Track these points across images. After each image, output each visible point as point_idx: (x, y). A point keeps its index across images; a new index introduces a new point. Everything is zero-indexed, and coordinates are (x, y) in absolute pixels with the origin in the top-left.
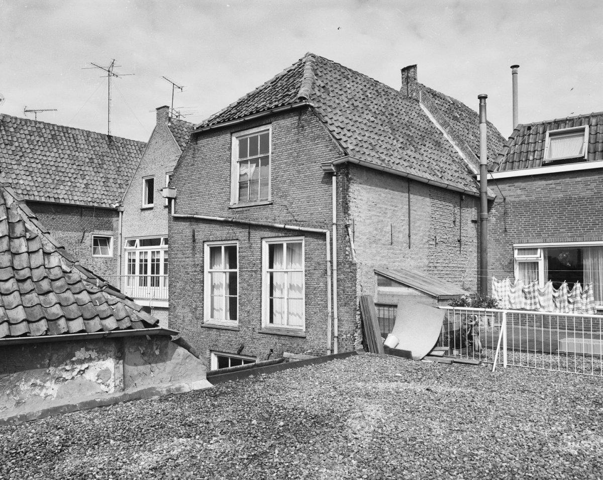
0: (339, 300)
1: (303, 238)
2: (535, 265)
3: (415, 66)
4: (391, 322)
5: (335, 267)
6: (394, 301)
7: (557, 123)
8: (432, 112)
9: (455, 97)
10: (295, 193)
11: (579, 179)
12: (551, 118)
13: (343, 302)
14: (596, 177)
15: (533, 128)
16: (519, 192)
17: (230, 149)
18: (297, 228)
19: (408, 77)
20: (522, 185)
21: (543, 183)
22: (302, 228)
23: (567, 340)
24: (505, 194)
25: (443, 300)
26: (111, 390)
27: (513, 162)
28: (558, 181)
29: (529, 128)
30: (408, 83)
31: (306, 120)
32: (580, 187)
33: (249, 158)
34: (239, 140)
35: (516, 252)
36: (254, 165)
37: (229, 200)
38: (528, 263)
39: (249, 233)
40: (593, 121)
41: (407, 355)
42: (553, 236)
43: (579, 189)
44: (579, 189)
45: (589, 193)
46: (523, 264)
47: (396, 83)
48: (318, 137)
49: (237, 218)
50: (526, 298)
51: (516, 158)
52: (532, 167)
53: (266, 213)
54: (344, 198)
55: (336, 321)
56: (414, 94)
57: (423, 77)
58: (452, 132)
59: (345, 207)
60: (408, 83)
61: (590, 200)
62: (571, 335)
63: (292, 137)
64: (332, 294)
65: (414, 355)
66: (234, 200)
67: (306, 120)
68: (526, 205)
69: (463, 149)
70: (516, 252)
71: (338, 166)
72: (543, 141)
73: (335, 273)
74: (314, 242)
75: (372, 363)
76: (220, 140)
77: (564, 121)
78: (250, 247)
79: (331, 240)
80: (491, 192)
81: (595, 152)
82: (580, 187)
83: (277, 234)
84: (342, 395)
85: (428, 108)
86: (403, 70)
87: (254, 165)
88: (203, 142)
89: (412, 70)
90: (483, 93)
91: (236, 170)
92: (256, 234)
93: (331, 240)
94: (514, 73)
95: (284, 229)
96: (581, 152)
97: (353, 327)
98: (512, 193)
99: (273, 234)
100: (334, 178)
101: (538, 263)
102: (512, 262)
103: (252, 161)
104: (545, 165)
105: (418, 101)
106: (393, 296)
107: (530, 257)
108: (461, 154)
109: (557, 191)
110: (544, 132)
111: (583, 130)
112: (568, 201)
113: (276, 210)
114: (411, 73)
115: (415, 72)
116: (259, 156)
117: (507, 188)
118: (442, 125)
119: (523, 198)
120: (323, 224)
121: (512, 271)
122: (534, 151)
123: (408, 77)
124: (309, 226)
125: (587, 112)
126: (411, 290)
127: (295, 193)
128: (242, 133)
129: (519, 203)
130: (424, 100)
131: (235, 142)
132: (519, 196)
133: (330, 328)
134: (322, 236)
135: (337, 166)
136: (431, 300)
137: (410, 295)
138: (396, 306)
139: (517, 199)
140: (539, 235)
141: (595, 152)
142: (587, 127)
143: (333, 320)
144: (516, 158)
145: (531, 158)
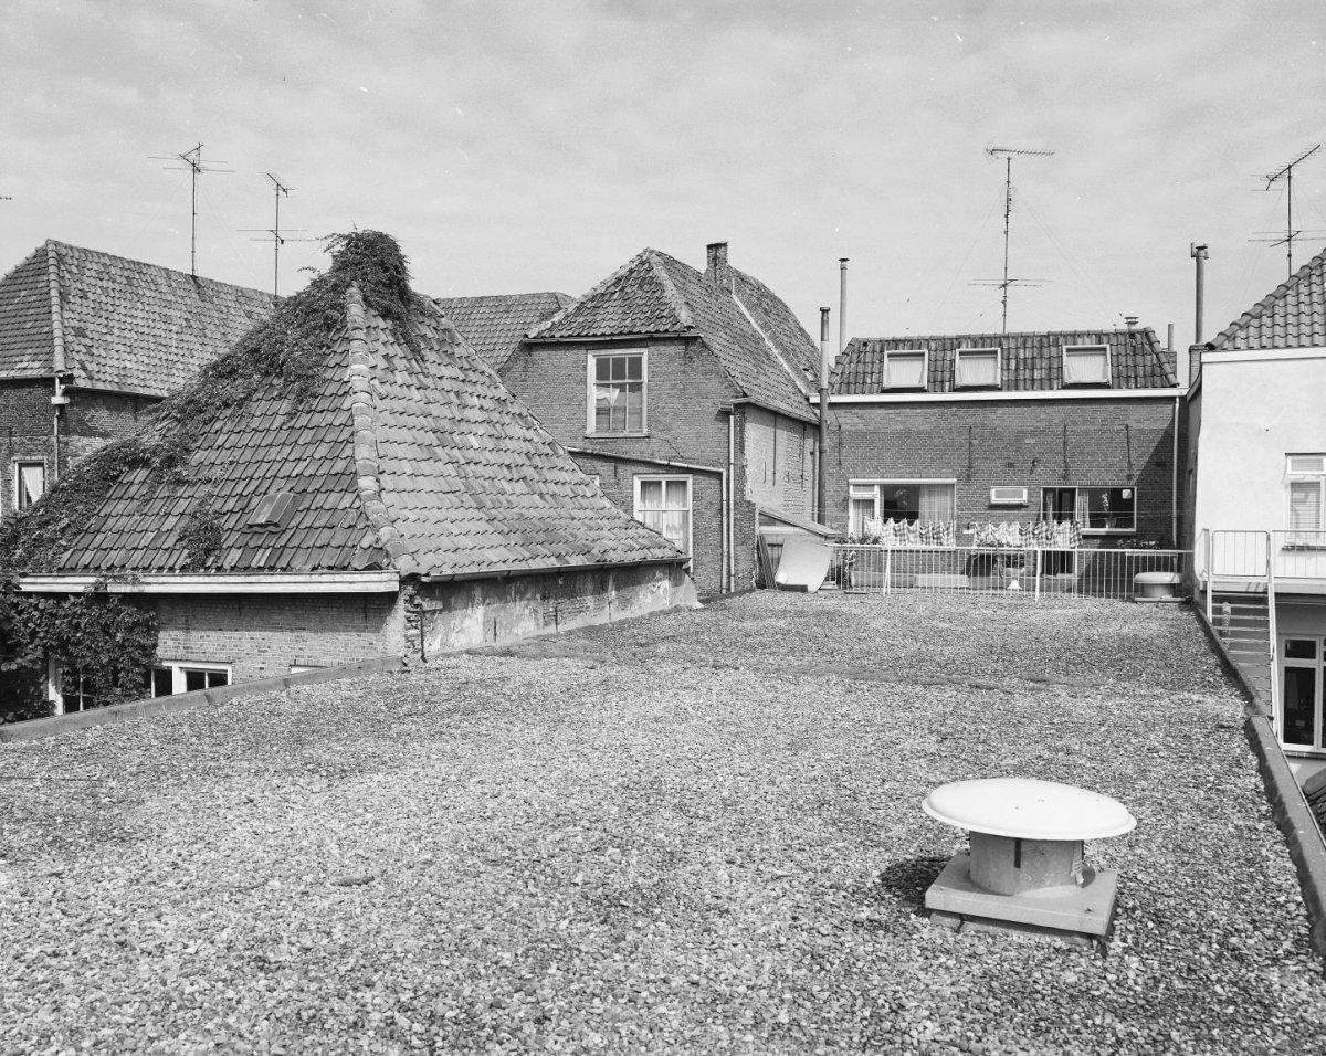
0: (735, 539)
1: (690, 476)
2: (870, 503)
3: (725, 245)
4: (775, 561)
5: (732, 507)
6: (779, 541)
7: (896, 342)
8: (749, 309)
9: (761, 280)
10: (679, 428)
11: (919, 411)
12: (889, 336)
13: (739, 541)
14: (936, 410)
15: (870, 345)
16: (856, 420)
17: (585, 368)
18: (686, 465)
19: (716, 258)
20: (860, 412)
21: (882, 412)
22: (690, 466)
23: (920, 576)
24: (841, 420)
25: (830, 538)
26: (666, 604)
27: (848, 384)
28: (898, 411)
29: (865, 344)
30: (716, 265)
31: (695, 352)
32: (920, 419)
33: (611, 381)
34: (597, 360)
35: (851, 487)
36: (618, 390)
37: (584, 427)
38: (863, 501)
39: (616, 468)
40: (933, 345)
41: (803, 589)
42: (893, 470)
43: (919, 421)
44: (919, 421)
45: (927, 427)
46: (857, 502)
47: (700, 263)
48: (711, 372)
49: (597, 449)
50: (896, 535)
51: (852, 379)
52: (871, 393)
53: (643, 445)
54: (742, 438)
55: (732, 560)
56: (725, 281)
57: (735, 259)
58: (773, 338)
59: (741, 446)
60: (716, 265)
61: (929, 435)
62: (924, 572)
63: (676, 366)
64: (729, 534)
65: (809, 589)
66: (591, 429)
67: (695, 352)
68: (863, 435)
69: (788, 361)
70: (851, 487)
71: (737, 406)
72: (882, 362)
73: (732, 515)
74: (705, 481)
75: (764, 598)
76: (571, 356)
77: (904, 341)
78: (617, 484)
79: (728, 479)
80: (830, 417)
81: (934, 382)
82: (920, 419)
83: (653, 471)
84: (23, 895)
85: (742, 301)
86: (710, 247)
87: (618, 390)
88: (541, 356)
89: (723, 249)
90: (826, 306)
91: (594, 394)
92: (625, 470)
93: (728, 479)
94: (843, 268)
95: (668, 465)
96: (921, 381)
97: (750, 565)
98: (848, 420)
99: (650, 470)
100: (732, 417)
101: (873, 501)
102: (846, 500)
103: (615, 386)
104: (885, 391)
105: (731, 292)
106: (777, 535)
107: (865, 494)
108: (786, 366)
109: (896, 422)
110: (882, 351)
111: (923, 355)
112: (907, 434)
113: (655, 444)
114: (720, 253)
115: (725, 252)
116: (627, 381)
117: (843, 415)
118: (762, 328)
119: (861, 426)
120: (718, 463)
121: (846, 509)
122: (872, 374)
123: (716, 258)
124: (698, 463)
125: (927, 334)
126: (797, 529)
127: (679, 428)
128: (603, 352)
129: (855, 433)
130: (738, 291)
131: (592, 361)
132: (856, 425)
133: (725, 567)
134: (719, 475)
135: (736, 405)
136: (818, 538)
137: (797, 534)
138: (782, 545)
139: (853, 429)
140: (876, 469)
141: (934, 382)
142: (926, 351)
143: (729, 559)
144: (852, 379)
145: (869, 381)
